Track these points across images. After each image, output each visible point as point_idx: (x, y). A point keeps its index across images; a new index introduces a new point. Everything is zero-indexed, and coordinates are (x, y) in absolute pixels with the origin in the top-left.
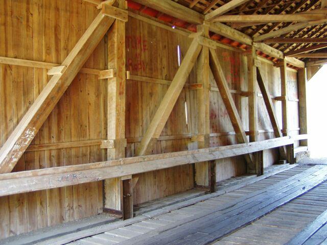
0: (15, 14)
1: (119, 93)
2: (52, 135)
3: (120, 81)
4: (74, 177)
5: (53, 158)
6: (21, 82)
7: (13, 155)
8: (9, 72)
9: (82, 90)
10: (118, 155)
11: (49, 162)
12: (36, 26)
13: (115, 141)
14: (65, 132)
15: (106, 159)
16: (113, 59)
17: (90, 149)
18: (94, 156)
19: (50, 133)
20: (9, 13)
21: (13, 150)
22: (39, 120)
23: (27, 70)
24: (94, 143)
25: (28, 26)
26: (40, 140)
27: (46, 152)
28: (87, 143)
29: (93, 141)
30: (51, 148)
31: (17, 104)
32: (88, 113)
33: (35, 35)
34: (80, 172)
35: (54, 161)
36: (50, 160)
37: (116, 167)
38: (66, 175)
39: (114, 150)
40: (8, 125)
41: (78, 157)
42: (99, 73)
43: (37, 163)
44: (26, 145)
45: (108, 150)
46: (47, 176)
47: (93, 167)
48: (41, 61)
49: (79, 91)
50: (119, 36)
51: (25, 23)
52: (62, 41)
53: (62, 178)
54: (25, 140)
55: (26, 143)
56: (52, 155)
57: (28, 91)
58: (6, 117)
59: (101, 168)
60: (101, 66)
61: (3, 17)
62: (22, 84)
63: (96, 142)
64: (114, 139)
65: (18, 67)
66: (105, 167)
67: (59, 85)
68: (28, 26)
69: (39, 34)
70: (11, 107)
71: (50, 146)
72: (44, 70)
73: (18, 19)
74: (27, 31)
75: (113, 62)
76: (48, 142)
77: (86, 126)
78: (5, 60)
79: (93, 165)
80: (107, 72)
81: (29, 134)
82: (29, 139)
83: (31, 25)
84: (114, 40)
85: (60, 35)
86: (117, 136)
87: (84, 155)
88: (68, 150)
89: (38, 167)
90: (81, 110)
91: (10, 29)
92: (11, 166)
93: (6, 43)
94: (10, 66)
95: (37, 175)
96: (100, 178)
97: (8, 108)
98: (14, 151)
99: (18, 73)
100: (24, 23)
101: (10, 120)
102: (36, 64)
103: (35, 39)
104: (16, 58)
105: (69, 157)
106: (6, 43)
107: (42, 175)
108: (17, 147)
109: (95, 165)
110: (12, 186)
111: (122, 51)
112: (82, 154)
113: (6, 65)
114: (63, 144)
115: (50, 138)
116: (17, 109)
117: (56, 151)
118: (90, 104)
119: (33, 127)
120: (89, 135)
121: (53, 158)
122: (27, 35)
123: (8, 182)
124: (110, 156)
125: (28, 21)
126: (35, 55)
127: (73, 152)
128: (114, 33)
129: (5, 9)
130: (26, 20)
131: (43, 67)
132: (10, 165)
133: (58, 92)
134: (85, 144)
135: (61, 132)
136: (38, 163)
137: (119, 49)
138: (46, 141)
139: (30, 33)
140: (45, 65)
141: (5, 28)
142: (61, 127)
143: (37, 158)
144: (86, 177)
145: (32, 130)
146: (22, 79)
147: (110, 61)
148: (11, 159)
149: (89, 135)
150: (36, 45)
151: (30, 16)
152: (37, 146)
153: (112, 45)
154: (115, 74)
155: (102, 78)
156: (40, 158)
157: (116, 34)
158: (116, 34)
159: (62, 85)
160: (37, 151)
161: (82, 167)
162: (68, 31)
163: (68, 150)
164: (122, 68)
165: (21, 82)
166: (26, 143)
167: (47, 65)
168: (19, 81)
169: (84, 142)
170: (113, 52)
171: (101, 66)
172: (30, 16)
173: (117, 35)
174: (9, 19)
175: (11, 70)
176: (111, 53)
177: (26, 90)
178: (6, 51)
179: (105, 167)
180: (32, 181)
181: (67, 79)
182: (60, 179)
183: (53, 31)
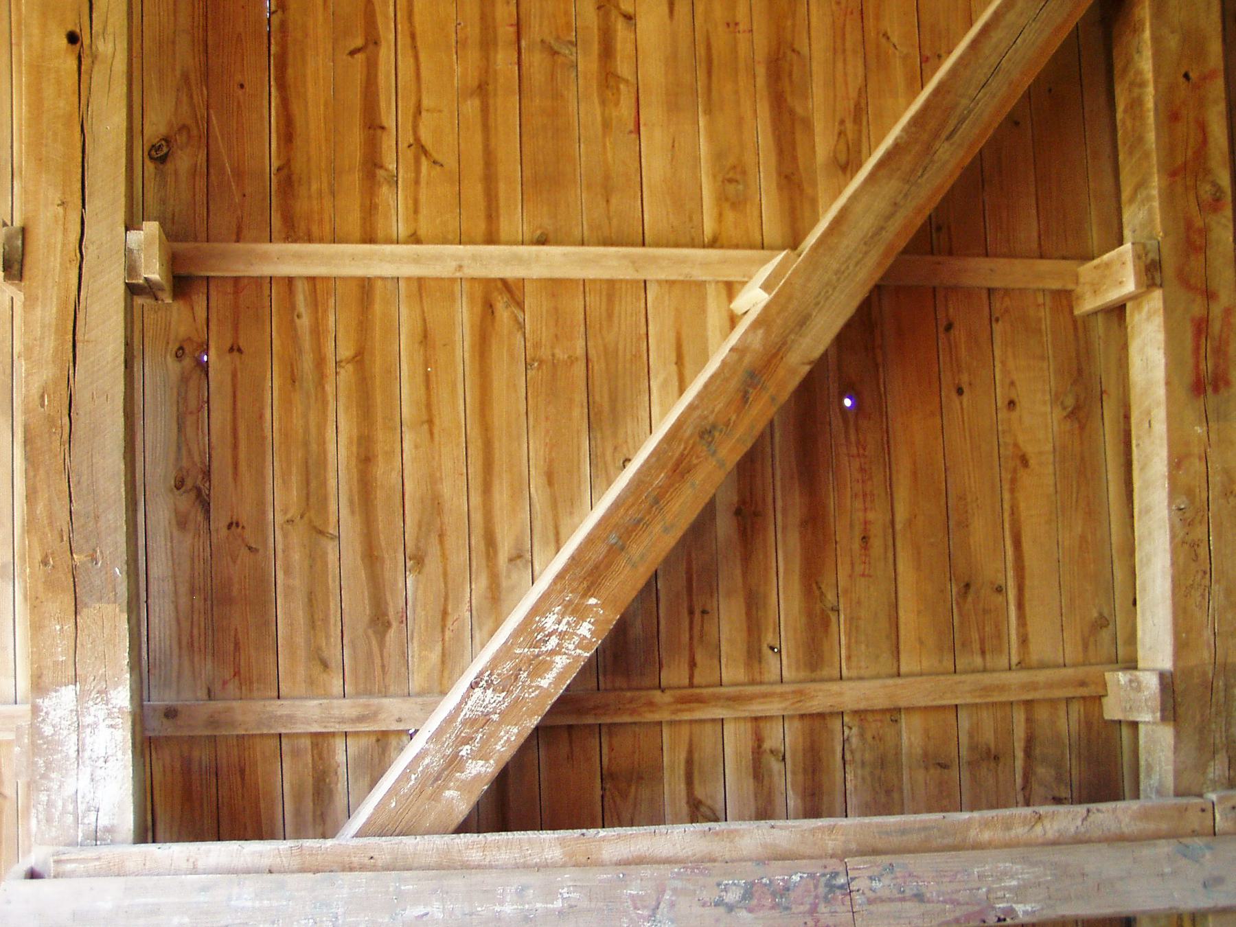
0: (536, 30)
1: (1188, 379)
2: (769, 638)
3: (1197, 309)
4: (831, 887)
5: (776, 766)
6: (572, 360)
7: (468, 740)
8: (504, 313)
9: (965, 378)
10: (1202, 768)
11: (749, 784)
12: (653, 72)
13: (1167, 683)
14: (851, 620)
15: (1136, 795)
16: (1142, 184)
17: (1029, 720)
18: (1058, 766)
19: (754, 627)
20: (506, 32)
21: (465, 712)
22: (622, 561)
23: (610, 298)
24: (1050, 685)
25: (608, 79)
26: (693, 664)
27: (729, 729)
28: (1002, 688)
29: (1042, 676)
30: (757, 708)
31: (550, 478)
32: (1014, 511)
33: (652, 114)
34: (885, 860)
35: (789, 793)
36: (758, 771)
37: (1164, 848)
38: (777, 875)
39: (1166, 734)
40: (505, 583)
41: (944, 766)
42: (1076, 278)
43: (673, 787)
44: (545, 693)
45: (1142, 728)
46: (647, 871)
47: (986, 836)
48: (694, 243)
49: (948, 392)
50: (1173, 42)
51: (594, 66)
52: (818, 126)
53: (748, 894)
54: (538, 666)
55: (544, 683)
56: (767, 745)
57: (613, 410)
58: (490, 541)
59: (1054, 843)
60: (352, 220)
61: (473, 55)
62: (579, 369)
63: (1063, 684)
64: (1167, 664)
65: (555, 287)
66: (1079, 840)
67: (747, 359)
68: (608, 79)
69: (673, 105)
70: (519, 489)
71: (751, 698)
72: (711, 291)
73: (555, 53)
74: (603, 103)
75: (1143, 203)
76: (740, 674)
77: (999, 590)
78: (474, 258)
79: (986, 824)
80: (1108, 265)
81: (562, 635)
82: (560, 662)
83: (623, 68)
84: (1139, 73)
85: (805, 95)
86: (1181, 646)
87: (993, 757)
88: (873, 727)
89: (684, 809)
90: (962, 498)
91: (506, 107)
92: (458, 801)
93: (489, 179)
94: (510, 289)
95: (590, 862)
96: (1020, 908)
97: (501, 495)
98: (471, 722)
99: (557, 315)
100: (588, 63)
101: (511, 560)
102: (654, 260)
103: (654, 140)
104: (542, 241)
105: (882, 762)
106: (489, 179)
107: (626, 863)
108: (489, 699)
109: (1008, 827)
110: (420, 910)
111: (1202, 127)
112: (973, 748)
113: (488, 282)
114: (835, 687)
115: (754, 655)
116: (554, 503)
117: (797, 724)
118: (1024, 461)
119: (586, 594)
120: (1024, 641)
121: (776, 766)
122: (606, 125)
123: (409, 883)
124: (1150, 768)
125: (607, 51)
126: (655, 215)
127: (911, 735)
128: (1137, 30)
129: (483, 18)
130: (595, 48)
131: (699, 275)
132: (448, 794)
133: (745, 398)
134: (986, 690)
135: (826, 623)
136: (682, 787)
137: (1174, 117)
138: (733, 671)
139: (625, 110)
140: (705, 264)
141: (485, 110)
142: (830, 597)
143: (673, 760)
144: (919, 897)
145: (579, 612)
146: (580, 343)
147: (1132, 200)
148: (454, 763)
149: (1024, 641)
150: (655, 167)
151: (620, 26)
152: (667, 697)
153: (1136, 104)
154: (1151, 272)
155: (1089, 304)
156: (689, 762)
157: (1147, 34)
158: (1147, 34)
159: (774, 355)
160: (672, 723)
161: (903, 831)
162: (855, 68)
163: (873, 727)
164: (1205, 231)
165: (572, 360)
166: (544, 683)
167: (724, 261)
168: (561, 355)
169: (987, 679)
170: (1141, 139)
171: (1095, 235)
172: (620, 26)
173: (1156, 39)
174: (503, 59)
175: (520, 305)
176: (1131, 153)
177: (602, 397)
178: (491, 215)
179: (1079, 840)
180: (550, 893)
181: (803, 321)
182: (732, 896)
183: (761, 80)
